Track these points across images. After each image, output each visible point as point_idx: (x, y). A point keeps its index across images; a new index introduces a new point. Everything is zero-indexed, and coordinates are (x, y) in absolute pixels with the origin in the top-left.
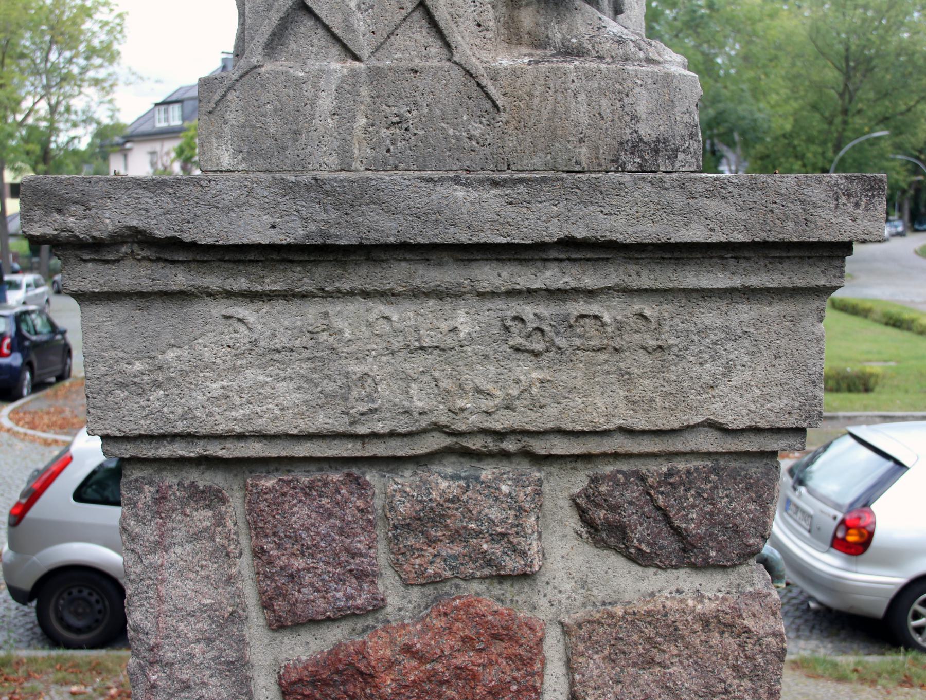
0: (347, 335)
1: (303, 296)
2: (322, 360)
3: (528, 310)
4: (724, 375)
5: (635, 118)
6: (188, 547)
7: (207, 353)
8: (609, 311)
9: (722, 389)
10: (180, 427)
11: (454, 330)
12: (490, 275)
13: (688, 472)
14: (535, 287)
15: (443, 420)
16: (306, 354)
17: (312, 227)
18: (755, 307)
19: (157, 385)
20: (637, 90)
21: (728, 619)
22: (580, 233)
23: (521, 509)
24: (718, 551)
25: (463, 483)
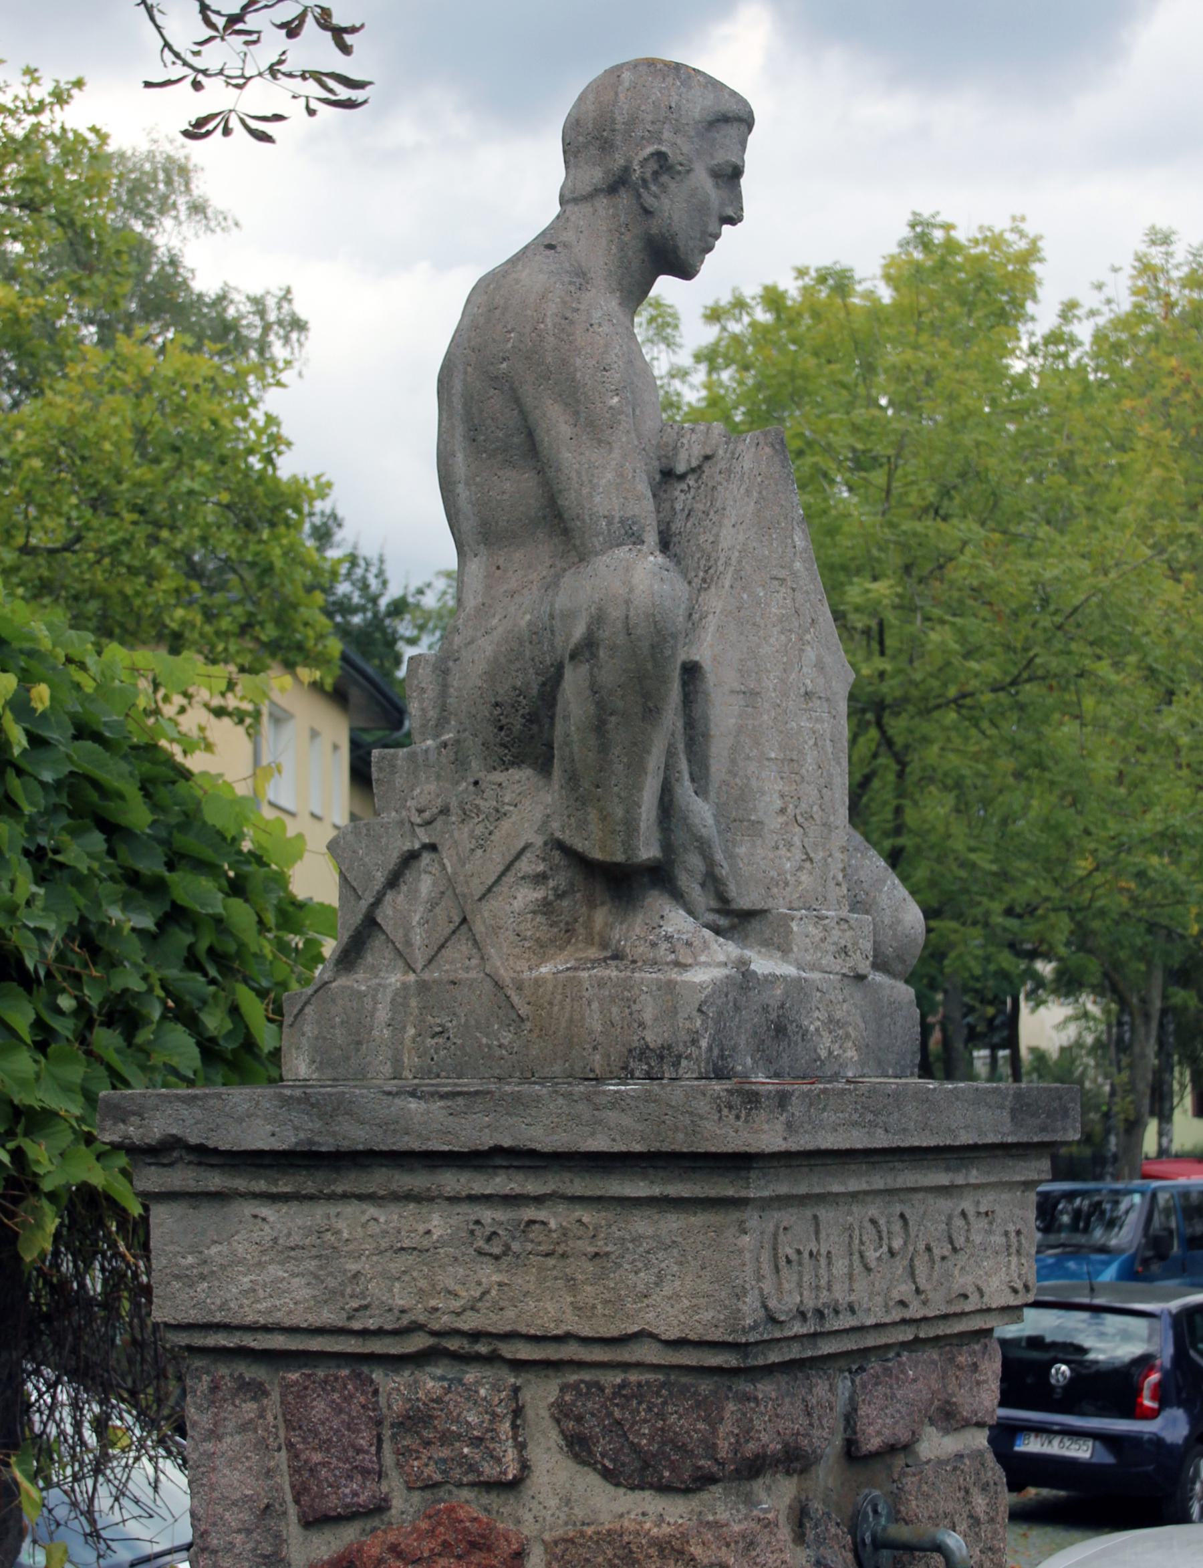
0: (345, 1235)
1: (311, 1198)
2: (327, 1258)
3: (488, 1215)
4: (657, 1284)
5: (642, 1025)
6: (238, 1438)
7: (241, 1250)
8: (554, 1217)
9: (655, 1298)
10: (218, 1318)
11: (428, 1232)
12: (452, 1181)
13: (639, 1385)
14: (487, 1192)
15: (422, 1319)
16: (314, 1252)
17: (302, 1135)
18: (682, 1216)
19: (203, 1277)
20: (643, 997)
21: (676, 1544)
22: (507, 1143)
23: (494, 1415)
24: (672, 1471)
25: (446, 1384)
